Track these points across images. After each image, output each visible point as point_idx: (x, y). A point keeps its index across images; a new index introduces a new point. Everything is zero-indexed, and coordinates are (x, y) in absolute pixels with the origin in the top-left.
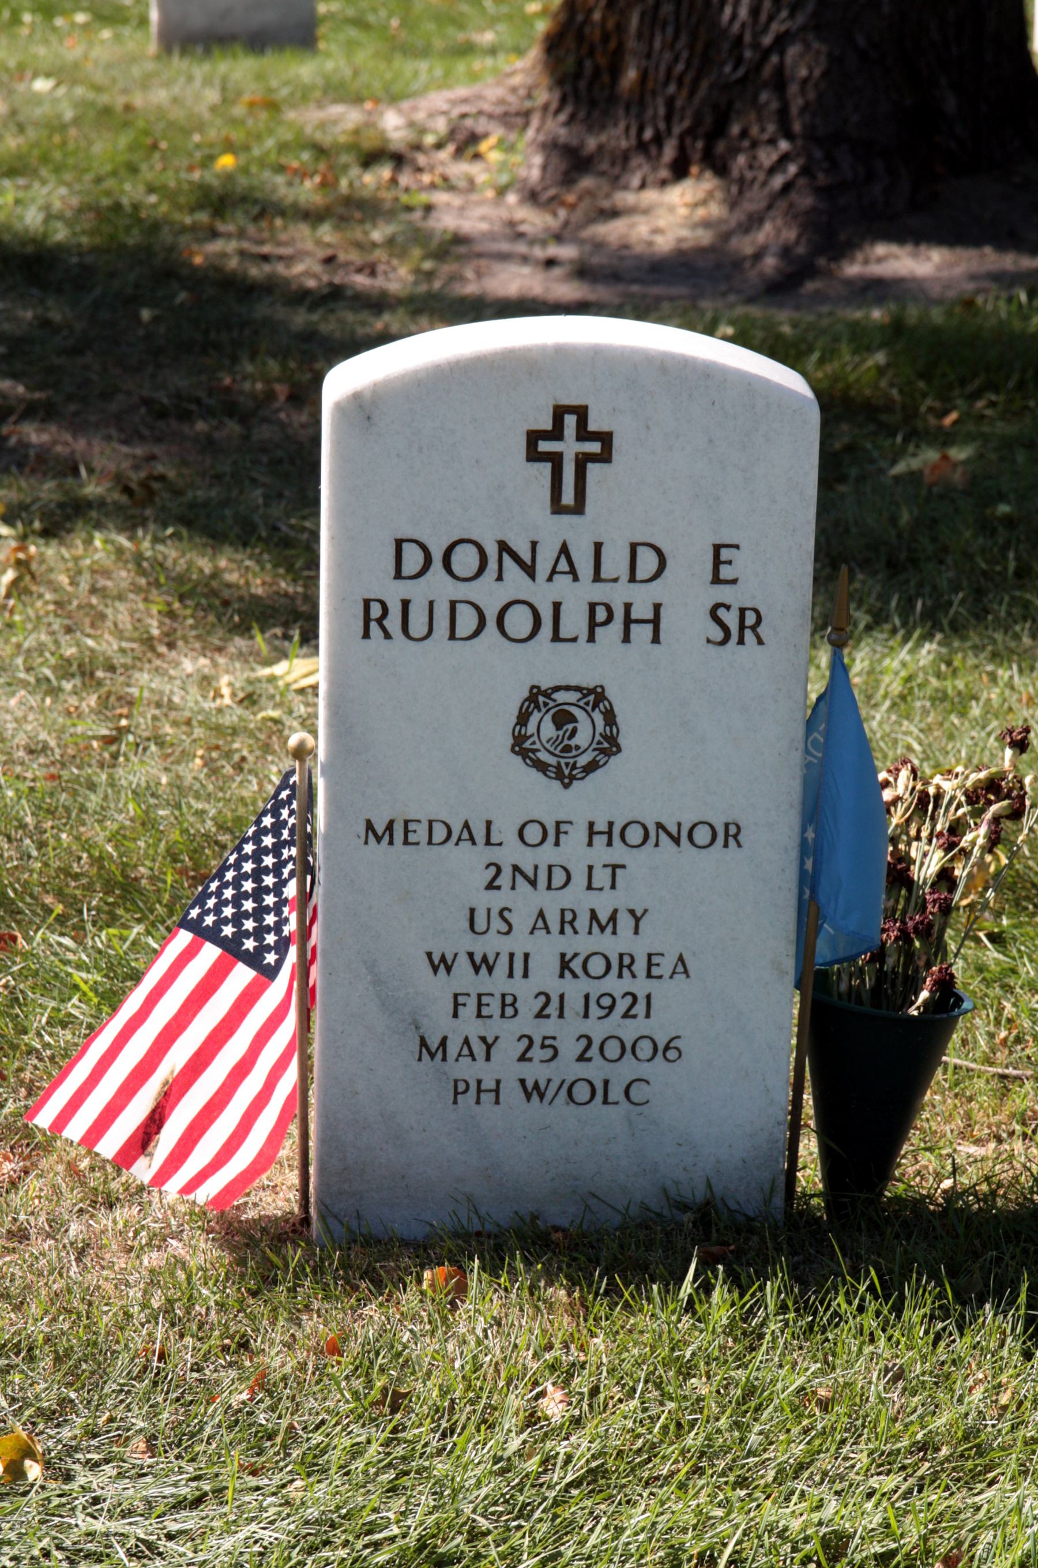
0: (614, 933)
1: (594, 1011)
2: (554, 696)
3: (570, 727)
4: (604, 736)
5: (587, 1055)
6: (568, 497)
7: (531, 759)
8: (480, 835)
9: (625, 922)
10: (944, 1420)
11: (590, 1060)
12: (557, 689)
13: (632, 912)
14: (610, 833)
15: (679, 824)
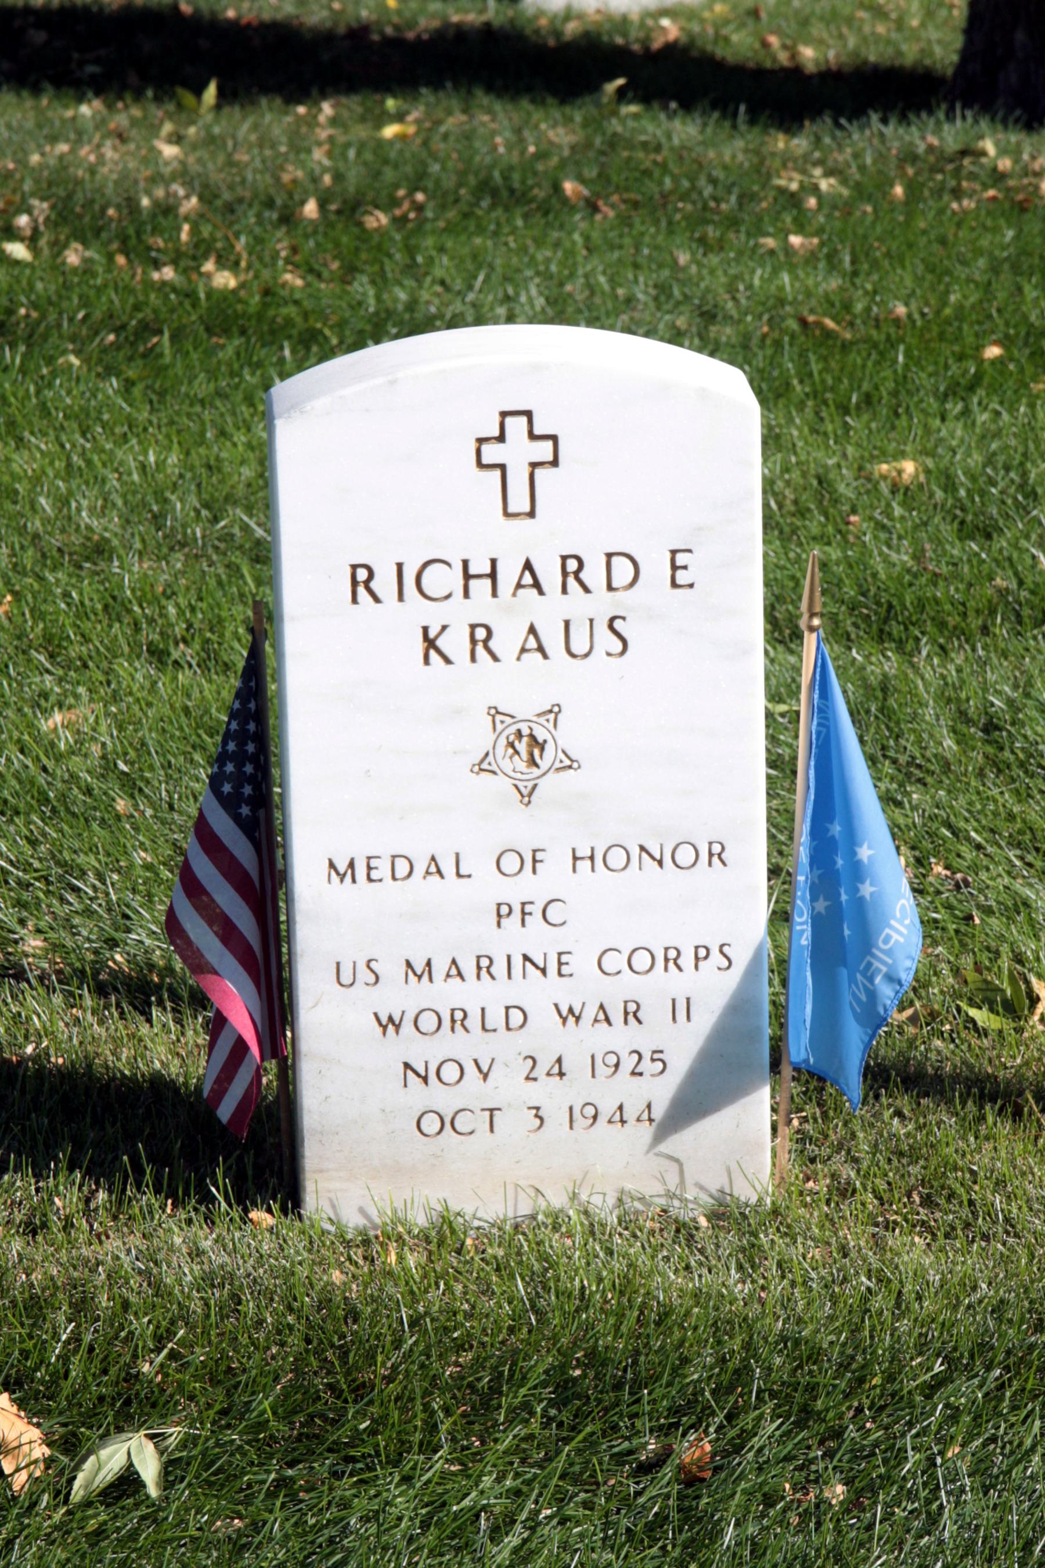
0: (431, 980)
1: (580, 1122)
6: (519, 502)
8: (448, 868)
14: (592, 858)
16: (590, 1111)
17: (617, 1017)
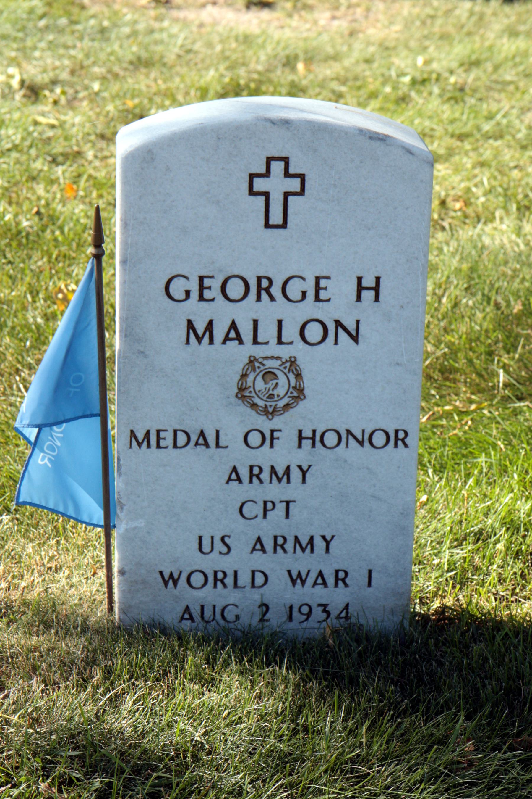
2: (265, 362)
3: (274, 382)
4: (294, 388)
6: (276, 218)
7: (248, 402)
8: (211, 440)
12: (266, 358)
14: (313, 439)
15: (363, 431)
17: (331, 581)
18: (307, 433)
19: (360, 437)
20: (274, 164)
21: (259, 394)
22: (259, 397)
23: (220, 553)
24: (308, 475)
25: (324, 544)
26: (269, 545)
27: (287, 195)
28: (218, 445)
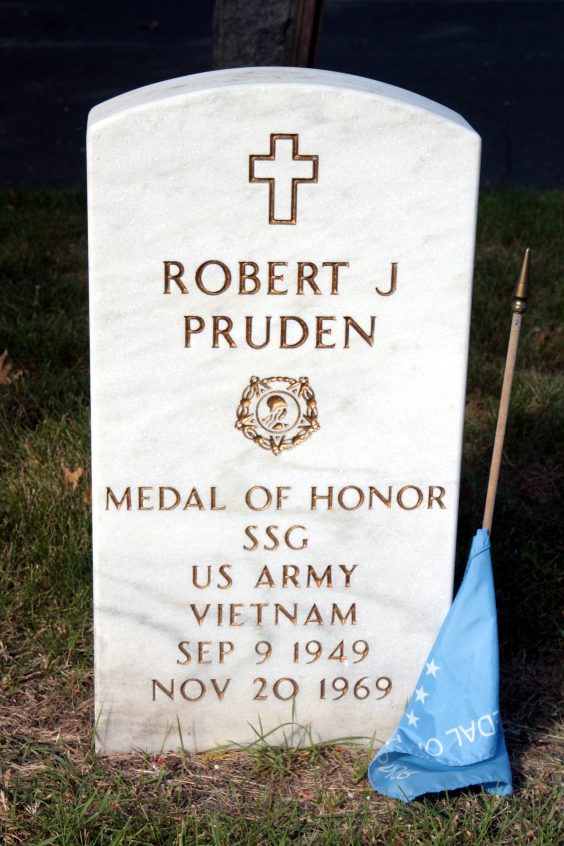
1: (330, 693)
4: (307, 417)
5: (263, 694)
6: (283, 212)
8: (206, 499)
9: (338, 576)
10: (33, 767)
11: (264, 698)
13: (343, 567)
16: (313, 648)
18: (322, 491)
19: (386, 496)
20: (279, 143)
21: (264, 423)
22: (263, 427)
23: (219, 586)
24: (352, 577)
25: (343, 575)
26: (277, 577)
27: (295, 182)
28: (213, 505)
